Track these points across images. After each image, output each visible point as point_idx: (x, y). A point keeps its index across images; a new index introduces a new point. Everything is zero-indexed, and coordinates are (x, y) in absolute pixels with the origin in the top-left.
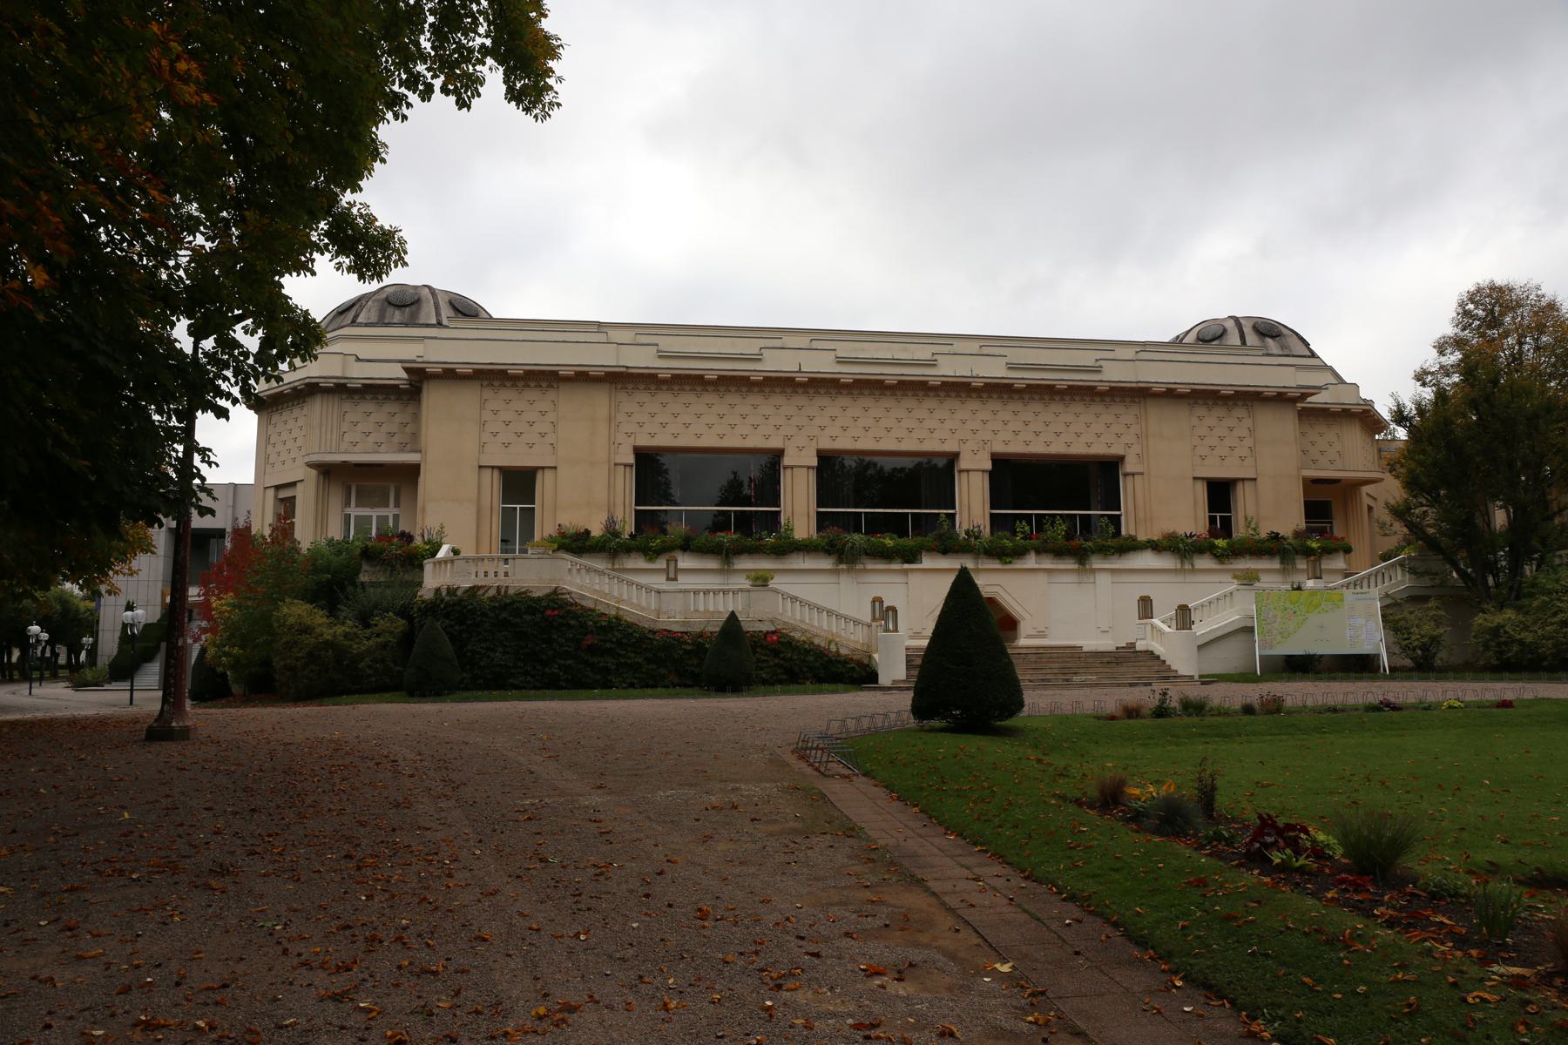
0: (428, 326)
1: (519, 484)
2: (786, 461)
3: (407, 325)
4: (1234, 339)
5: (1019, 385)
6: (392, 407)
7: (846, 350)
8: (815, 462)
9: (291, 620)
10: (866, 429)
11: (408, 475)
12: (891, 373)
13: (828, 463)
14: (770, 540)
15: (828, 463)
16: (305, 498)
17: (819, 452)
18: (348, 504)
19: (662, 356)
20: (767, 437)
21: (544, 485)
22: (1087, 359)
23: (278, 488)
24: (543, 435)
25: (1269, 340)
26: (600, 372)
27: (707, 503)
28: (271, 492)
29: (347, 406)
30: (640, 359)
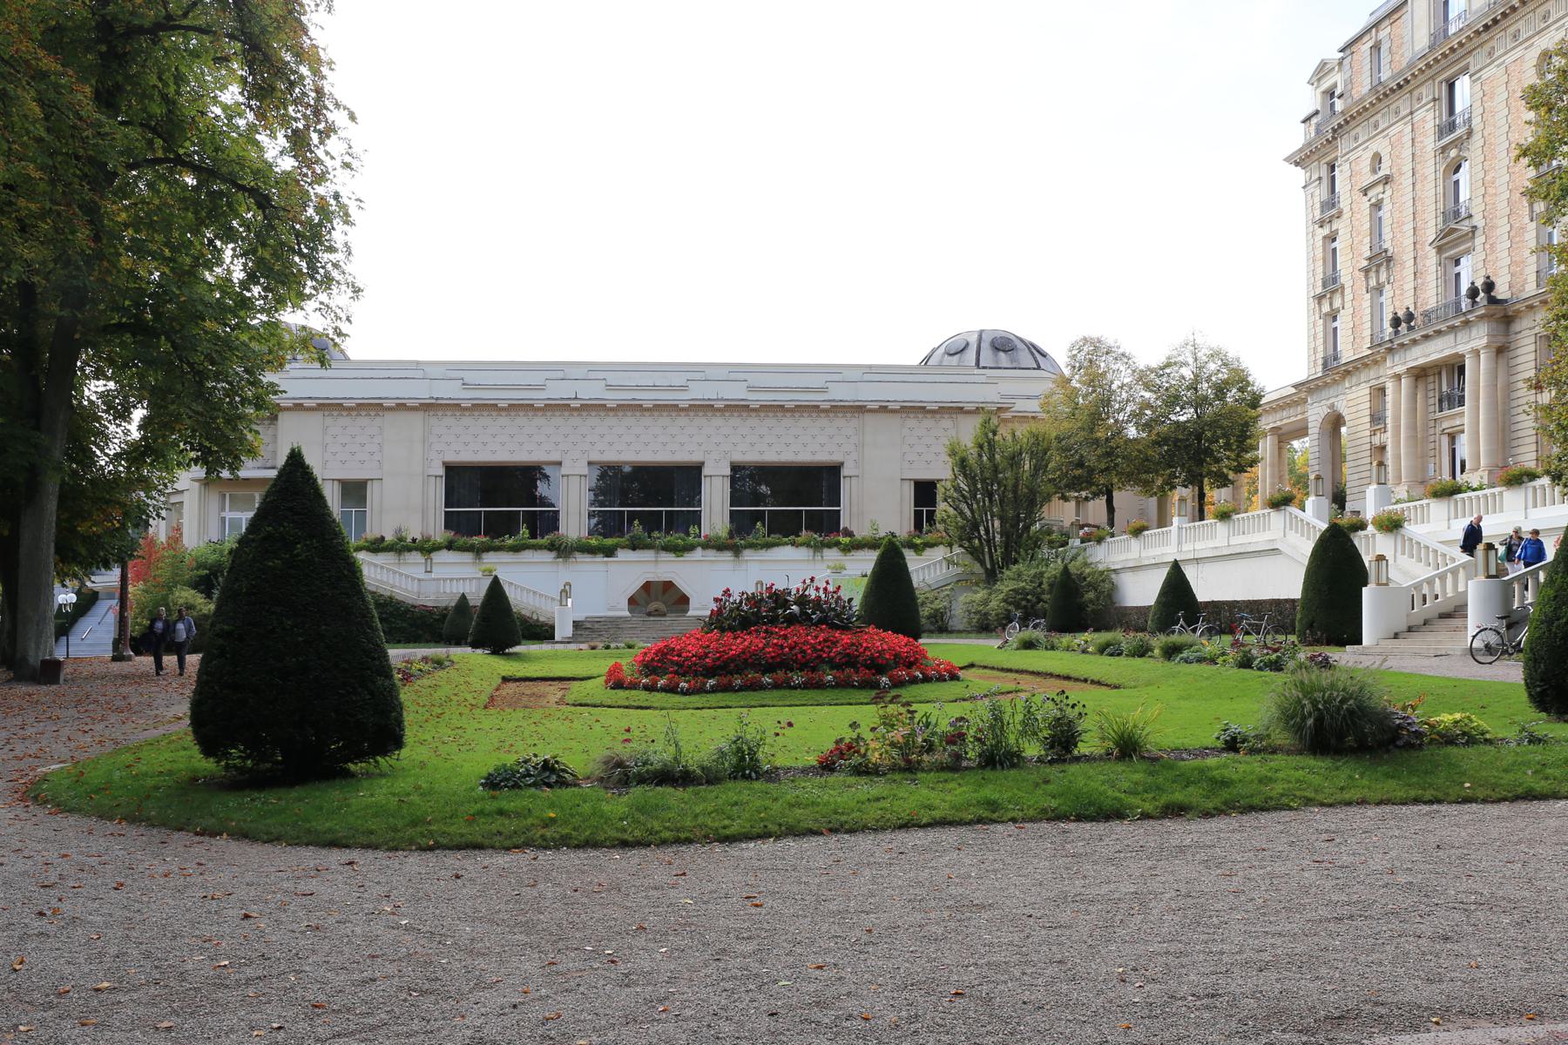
2: (705, 471)
4: (970, 356)
7: (613, 379)
9: (181, 601)
10: (629, 444)
12: (647, 397)
13: (739, 472)
14: (510, 542)
15: (739, 472)
18: (223, 509)
20: (548, 452)
21: (372, 492)
22: (817, 381)
24: (372, 454)
25: (1002, 354)
26: (416, 403)
30: (449, 391)
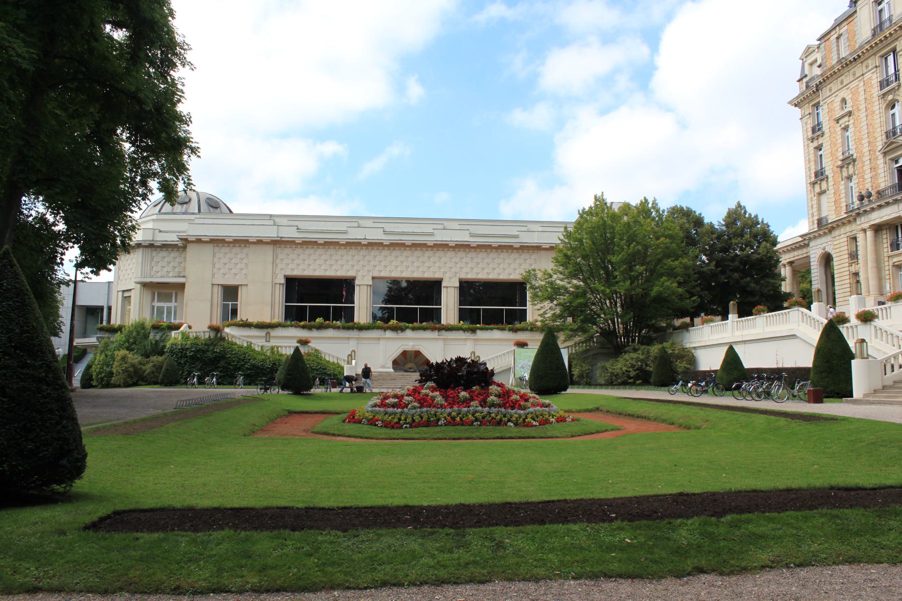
0: (193, 214)
1: (230, 292)
3: (184, 214)
4: (193, 207)
5: (494, 245)
6: (174, 254)
7: (389, 227)
8: (458, 285)
11: (182, 286)
16: (135, 296)
17: (285, 276)
18: (153, 300)
19: (472, 235)
21: (242, 293)
23: (124, 291)
26: (268, 240)
27: (316, 300)
28: (120, 293)
29: (154, 253)
